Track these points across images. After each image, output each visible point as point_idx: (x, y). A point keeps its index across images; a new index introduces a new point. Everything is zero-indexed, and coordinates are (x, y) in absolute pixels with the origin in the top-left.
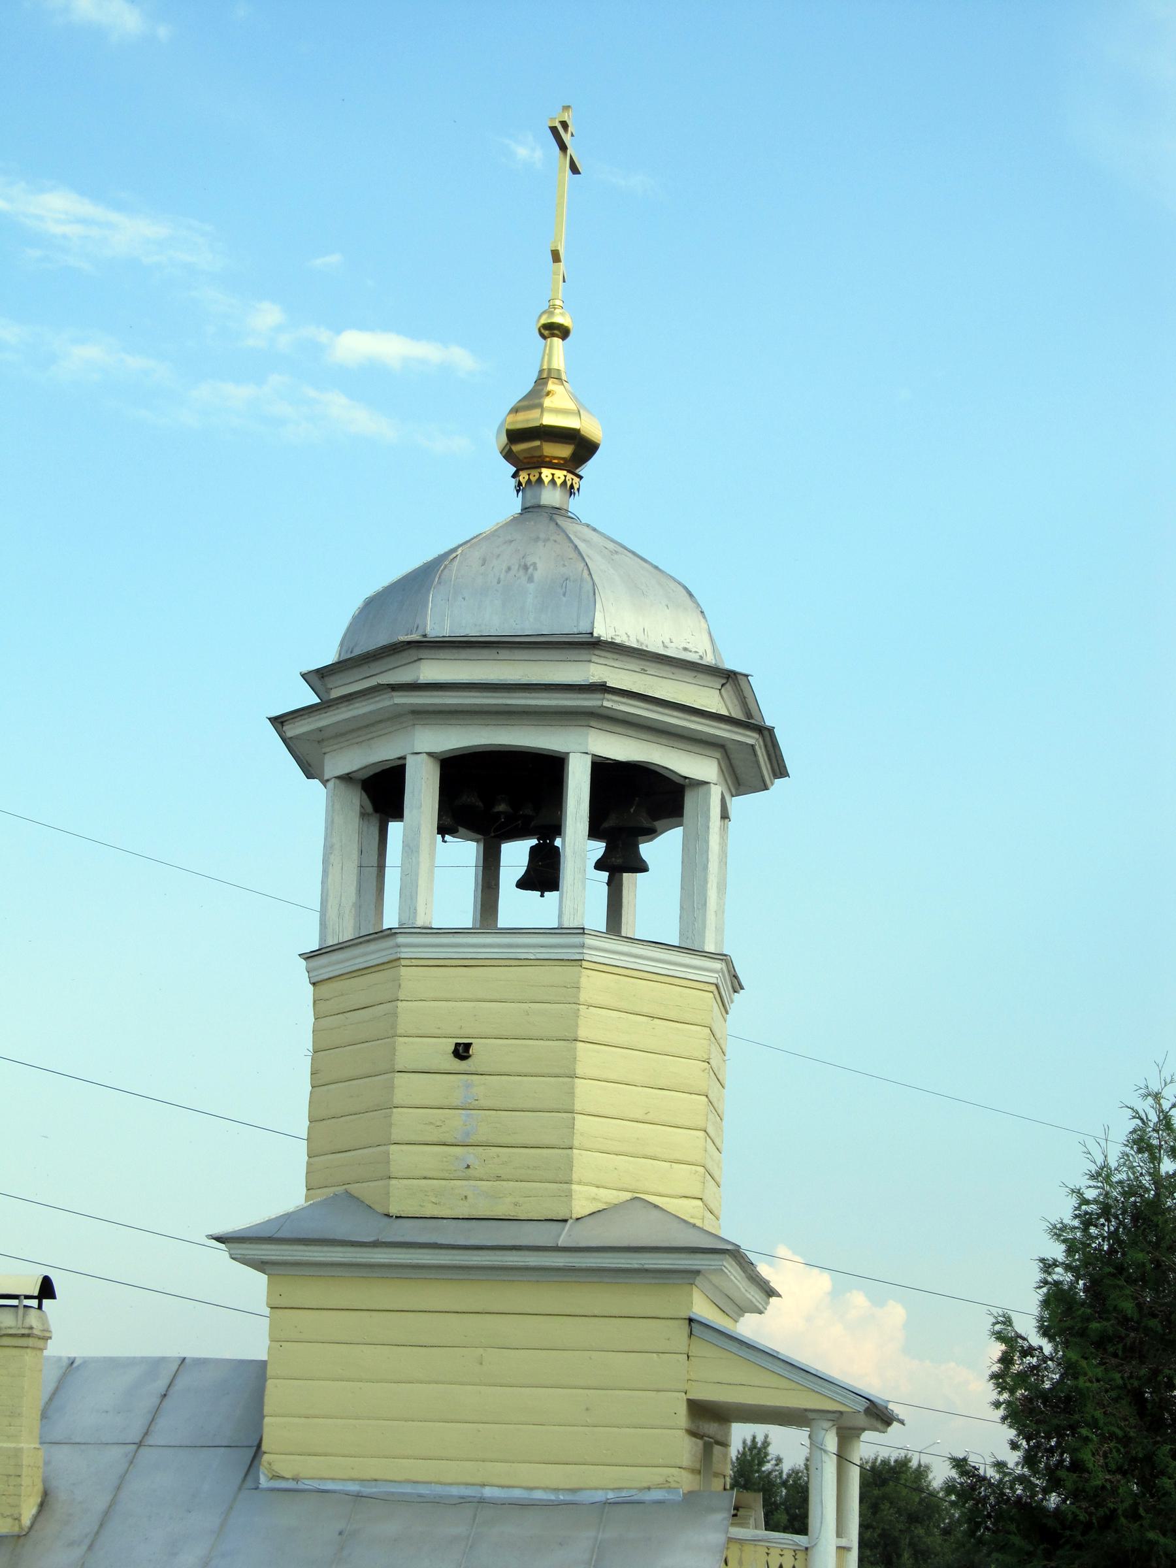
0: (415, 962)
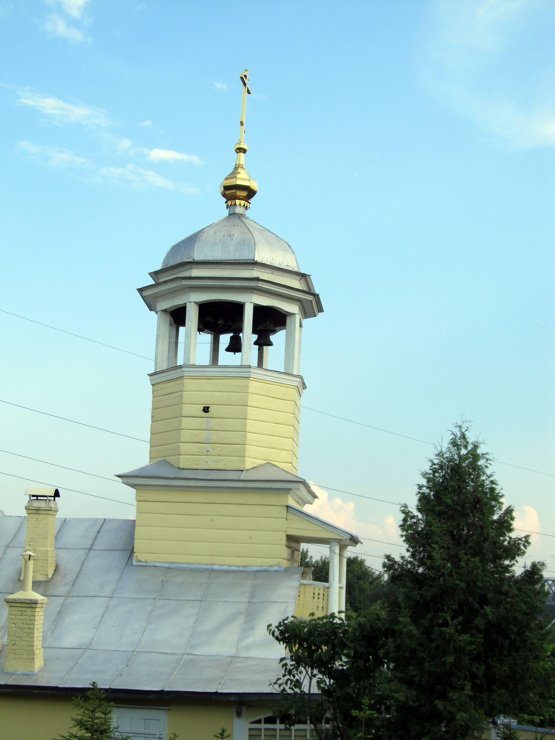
0: (189, 377)
